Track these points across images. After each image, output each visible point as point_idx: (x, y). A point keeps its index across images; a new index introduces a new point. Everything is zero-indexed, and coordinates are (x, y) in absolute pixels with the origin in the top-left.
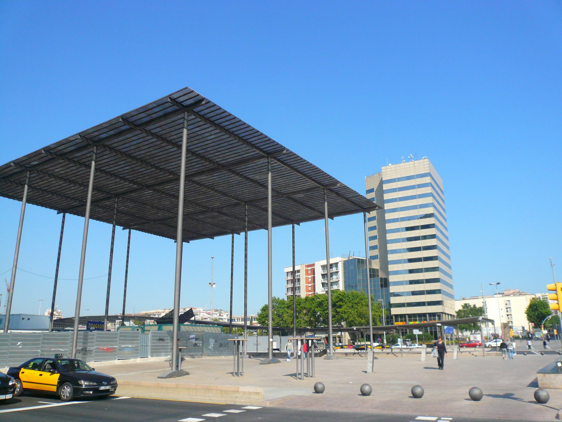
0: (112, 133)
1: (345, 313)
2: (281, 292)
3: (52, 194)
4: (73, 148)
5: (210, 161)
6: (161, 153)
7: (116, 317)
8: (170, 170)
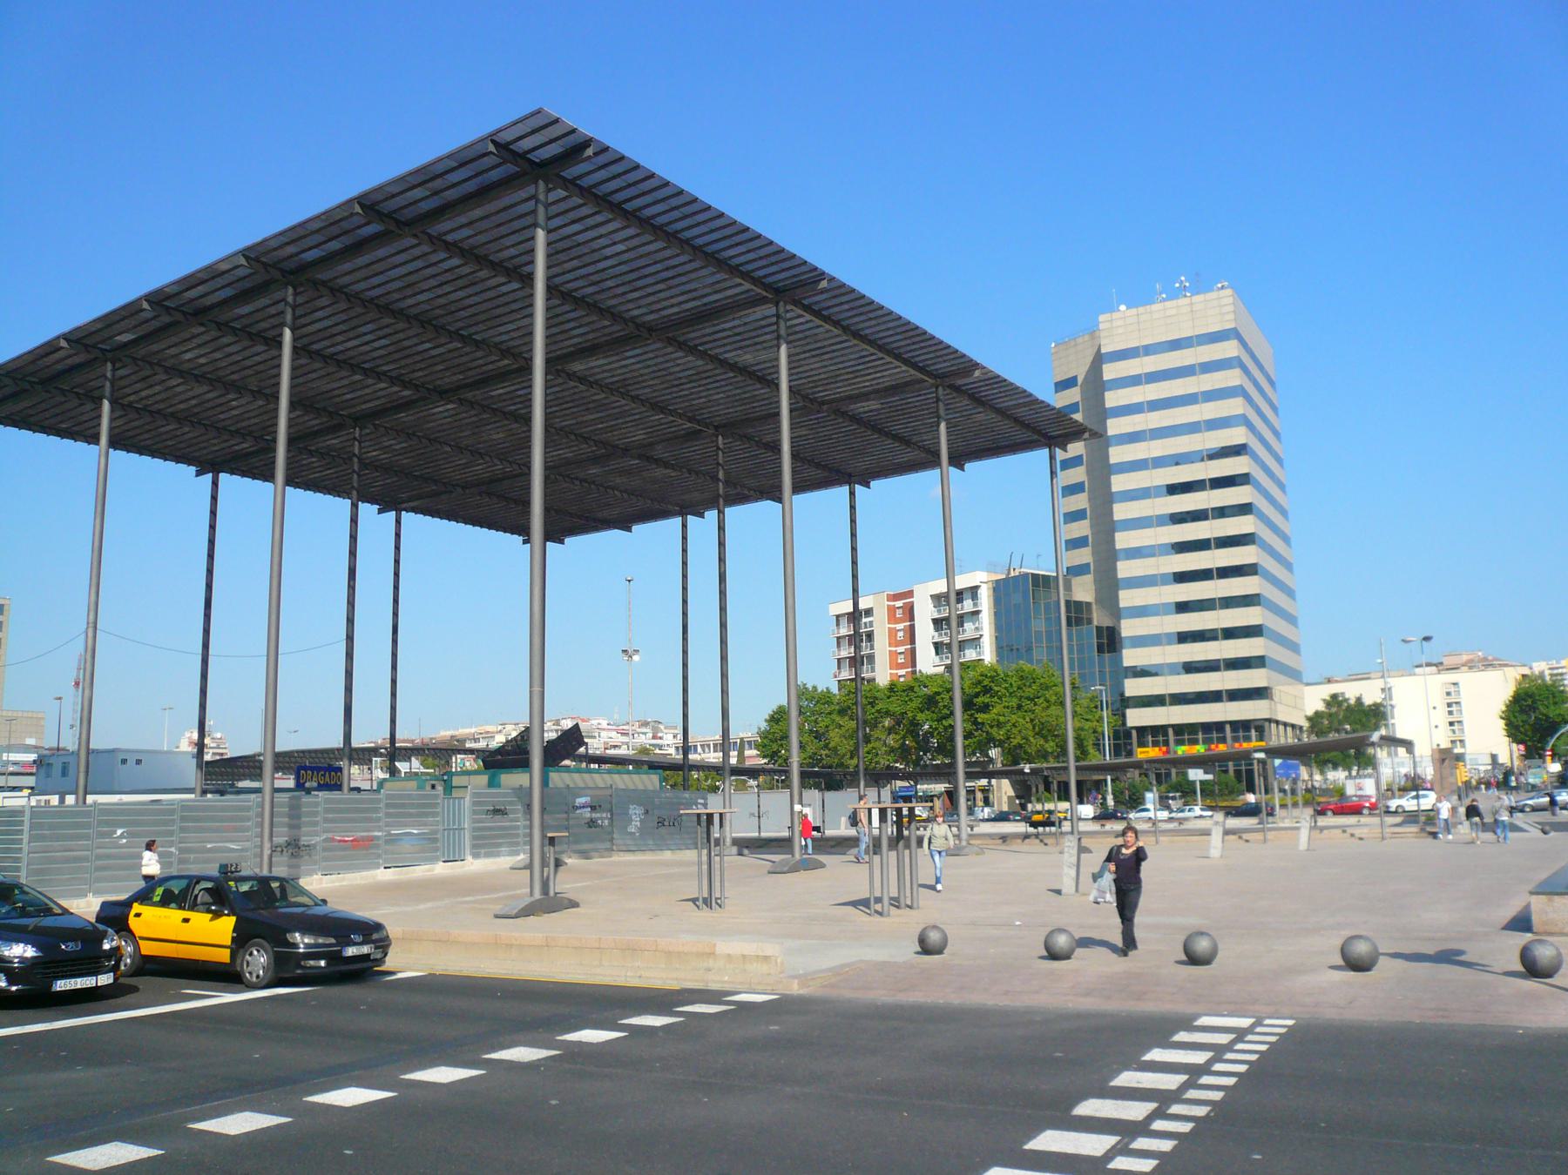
0: (335, 245)
1: (999, 725)
2: (823, 672)
3: (179, 420)
4: (229, 292)
5: (616, 317)
6: (477, 299)
7: (374, 751)
8: (497, 340)
